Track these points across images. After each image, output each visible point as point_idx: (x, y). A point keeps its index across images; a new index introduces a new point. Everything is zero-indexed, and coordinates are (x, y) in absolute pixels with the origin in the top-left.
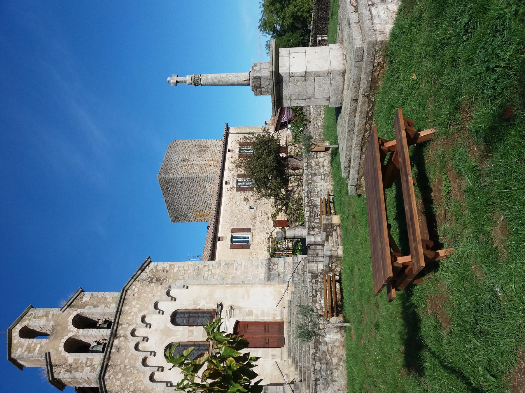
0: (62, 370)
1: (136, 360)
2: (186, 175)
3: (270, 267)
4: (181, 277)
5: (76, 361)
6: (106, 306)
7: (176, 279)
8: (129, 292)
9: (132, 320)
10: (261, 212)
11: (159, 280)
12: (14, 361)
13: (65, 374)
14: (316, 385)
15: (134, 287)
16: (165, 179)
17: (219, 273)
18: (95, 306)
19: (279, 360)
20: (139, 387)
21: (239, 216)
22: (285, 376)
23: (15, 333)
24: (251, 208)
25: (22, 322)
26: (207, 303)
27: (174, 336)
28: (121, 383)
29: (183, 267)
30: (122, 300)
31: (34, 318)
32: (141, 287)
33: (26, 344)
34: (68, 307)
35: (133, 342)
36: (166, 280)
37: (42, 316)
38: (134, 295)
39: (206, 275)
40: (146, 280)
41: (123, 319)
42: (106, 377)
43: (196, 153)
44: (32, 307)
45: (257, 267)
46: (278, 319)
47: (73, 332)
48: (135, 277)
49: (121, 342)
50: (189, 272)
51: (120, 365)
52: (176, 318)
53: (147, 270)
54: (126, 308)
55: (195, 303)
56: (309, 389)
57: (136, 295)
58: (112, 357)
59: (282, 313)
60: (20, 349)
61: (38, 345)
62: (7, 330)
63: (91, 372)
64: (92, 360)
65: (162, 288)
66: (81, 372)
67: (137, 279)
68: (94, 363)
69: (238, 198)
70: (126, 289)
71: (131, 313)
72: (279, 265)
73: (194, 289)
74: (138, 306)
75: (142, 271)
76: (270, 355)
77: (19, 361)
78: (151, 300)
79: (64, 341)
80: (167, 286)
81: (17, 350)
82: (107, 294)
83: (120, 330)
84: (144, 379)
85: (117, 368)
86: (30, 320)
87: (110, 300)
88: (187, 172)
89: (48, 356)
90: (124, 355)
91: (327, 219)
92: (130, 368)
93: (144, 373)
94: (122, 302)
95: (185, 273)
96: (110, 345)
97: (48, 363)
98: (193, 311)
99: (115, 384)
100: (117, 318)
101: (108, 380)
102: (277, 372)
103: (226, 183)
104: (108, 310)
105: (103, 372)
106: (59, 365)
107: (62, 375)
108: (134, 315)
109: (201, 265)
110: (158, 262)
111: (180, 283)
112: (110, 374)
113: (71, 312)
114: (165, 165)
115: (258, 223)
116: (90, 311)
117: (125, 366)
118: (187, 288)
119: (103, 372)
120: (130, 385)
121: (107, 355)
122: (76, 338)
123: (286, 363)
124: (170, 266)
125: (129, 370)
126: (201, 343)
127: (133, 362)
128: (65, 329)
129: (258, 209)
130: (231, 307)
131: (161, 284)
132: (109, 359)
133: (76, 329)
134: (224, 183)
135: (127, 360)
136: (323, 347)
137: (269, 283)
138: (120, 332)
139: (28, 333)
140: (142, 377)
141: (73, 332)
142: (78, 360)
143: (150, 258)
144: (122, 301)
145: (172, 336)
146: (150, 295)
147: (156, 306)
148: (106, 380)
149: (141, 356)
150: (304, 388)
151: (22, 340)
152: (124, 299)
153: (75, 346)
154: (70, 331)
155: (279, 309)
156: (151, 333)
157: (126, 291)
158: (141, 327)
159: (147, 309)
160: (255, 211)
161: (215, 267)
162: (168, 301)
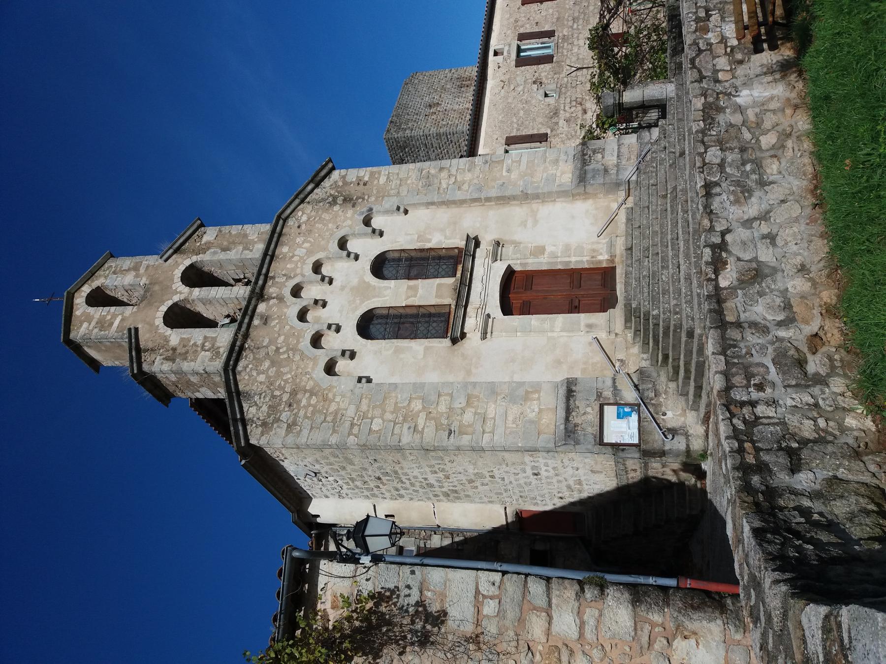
0: (158, 358)
1: (298, 338)
2: (433, 130)
3: (583, 158)
4: (392, 192)
5: (184, 342)
6: (245, 248)
7: (383, 194)
8: (291, 222)
9: (294, 269)
10: (568, 100)
11: (349, 200)
12: (76, 348)
13: (162, 363)
14: (708, 195)
15: (300, 213)
16: (397, 141)
17: (470, 180)
18: (225, 249)
19: (602, 335)
20: (303, 383)
21: (522, 113)
22: (617, 364)
23: (80, 300)
24: (546, 95)
25: (93, 281)
26: (446, 238)
27: (378, 296)
28: (268, 377)
29: (398, 174)
30: (276, 235)
31: (114, 273)
32: (313, 213)
33: (97, 316)
34: (175, 252)
35: (293, 307)
36: (363, 199)
37: (129, 270)
38: (299, 227)
39: (444, 185)
40: (323, 200)
41: (277, 268)
42: (239, 368)
43: (453, 90)
44: (112, 256)
45: (556, 161)
46: (603, 258)
47: (181, 292)
48: (302, 196)
49: (271, 307)
50: (409, 182)
51: (267, 347)
52: (381, 266)
53: (327, 183)
54: (284, 250)
55: (420, 238)
56: (677, 380)
57: (303, 227)
58: (253, 333)
59: (611, 245)
60: (85, 325)
61: (117, 319)
62: (65, 294)
63: (211, 360)
64: (214, 340)
65: (354, 213)
66: (192, 361)
67: (308, 200)
68: (218, 344)
69: (520, 80)
70: (283, 216)
71: (292, 257)
72: (607, 153)
73: (420, 216)
74: (306, 245)
75: (317, 185)
76: (582, 324)
77: (86, 349)
78: (331, 235)
79: (164, 308)
80: (365, 209)
81: (81, 326)
82: (248, 228)
83: (270, 287)
84: (313, 369)
85: (262, 353)
86: (106, 277)
87: (253, 237)
88: (436, 123)
89: (134, 334)
90: (276, 329)
91: (699, 295)
92: (286, 352)
93: (315, 359)
94: (275, 239)
95: (400, 185)
96: (249, 312)
97: (134, 345)
98: (419, 255)
99: (255, 380)
100: (266, 266)
101: (243, 374)
102: (600, 357)
103: (496, 54)
104: (248, 255)
105: (233, 358)
106: (153, 350)
107: (158, 366)
108: (299, 261)
109: (434, 168)
110: (347, 168)
111: (390, 203)
112: (247, 362)
113: (179, 260)
114: (398, 116)
115: (562, 122)
116: (216, 258)
117: (278, 349)
118: (406, 212)
119: (233, 358)
120: (286, 381)
121: (243, 329)
122: (188, 306)
123: (619, 339)
124: (372, 174)
125: (286, 356)
126: (433, 311)
127: (293, 341)
128: (167, 289)
129: (563, 96)
130: (498, 243)
131: (353, 206)
132: (246, 336)
133: (186, 289)
134: (491, 53)
135: (282, 338)
136: (729, 117)
137: (581, 190)
138: (271, 290)
139: (99, 298)
140: (310, 366)
141: (181, 292)
142: (189, 340)
143: (330, 160)
144: (275, 238)
145: (374, 297)
146: (330, 225)
147: (342, 244)
148: (240, 373)
149: (309, 330)
150: (663, 378)
151: (91, 310)
152: (280, 235)
153: (181, 317)
154: (177, 293)
155: (604, 240)
156: (332, 292)
157: (285, 220)
158: (311, 282)
159: (325, 249)
160: (557, 101)
161: (464, 170)
162: (365, 234)
